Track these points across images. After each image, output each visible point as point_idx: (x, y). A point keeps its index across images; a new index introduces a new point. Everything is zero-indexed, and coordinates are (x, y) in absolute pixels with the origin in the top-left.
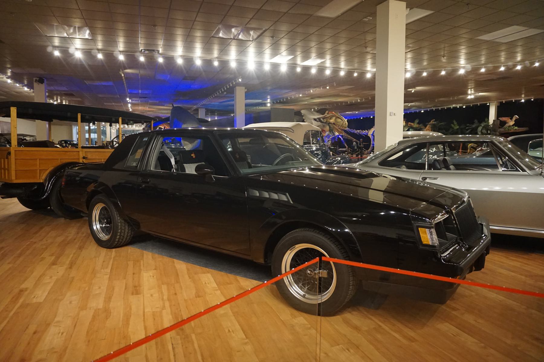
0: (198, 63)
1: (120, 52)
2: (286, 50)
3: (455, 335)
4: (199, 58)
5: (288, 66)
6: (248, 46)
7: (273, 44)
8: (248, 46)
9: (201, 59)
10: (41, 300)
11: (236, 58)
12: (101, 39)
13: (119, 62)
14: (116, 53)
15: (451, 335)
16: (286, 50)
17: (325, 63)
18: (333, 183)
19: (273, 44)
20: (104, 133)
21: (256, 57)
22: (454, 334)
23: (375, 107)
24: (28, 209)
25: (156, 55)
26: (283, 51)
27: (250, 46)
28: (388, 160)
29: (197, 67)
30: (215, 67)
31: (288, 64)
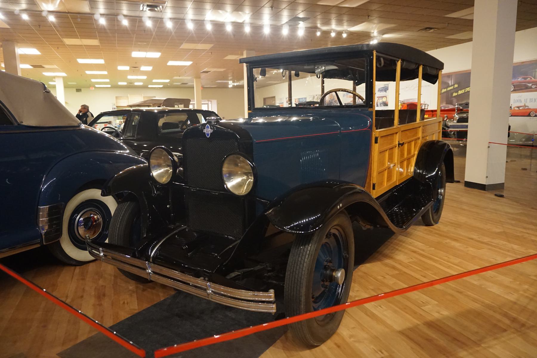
0: (267, 31)
1: (101, 15)
2: (305, 10)
3: (425, 302)
4: (210, 22)
5: (306, 30)
6: (263, 7)
7: (291, 3)
8: (263, 7)
9: (212, 23)
10: (533, 87)
11: (251, 22)
12: (268, 13)
13: (245, 33)
14: (97, 16)
15: (420, 302)
16: (305, 10)
17: (205, 15)
18: (433, 122)
19: (291, 3)
20: (105, 130)
21: (250, 18)
22: (424, 302)
23: (189, 99)
24: (113, 213)
25: (120, 18)
26: (300, 11)
27: (265, 6)
28: (108, 238)
29: (306, 36)
30: (347, 35)
31: (306, 28)
